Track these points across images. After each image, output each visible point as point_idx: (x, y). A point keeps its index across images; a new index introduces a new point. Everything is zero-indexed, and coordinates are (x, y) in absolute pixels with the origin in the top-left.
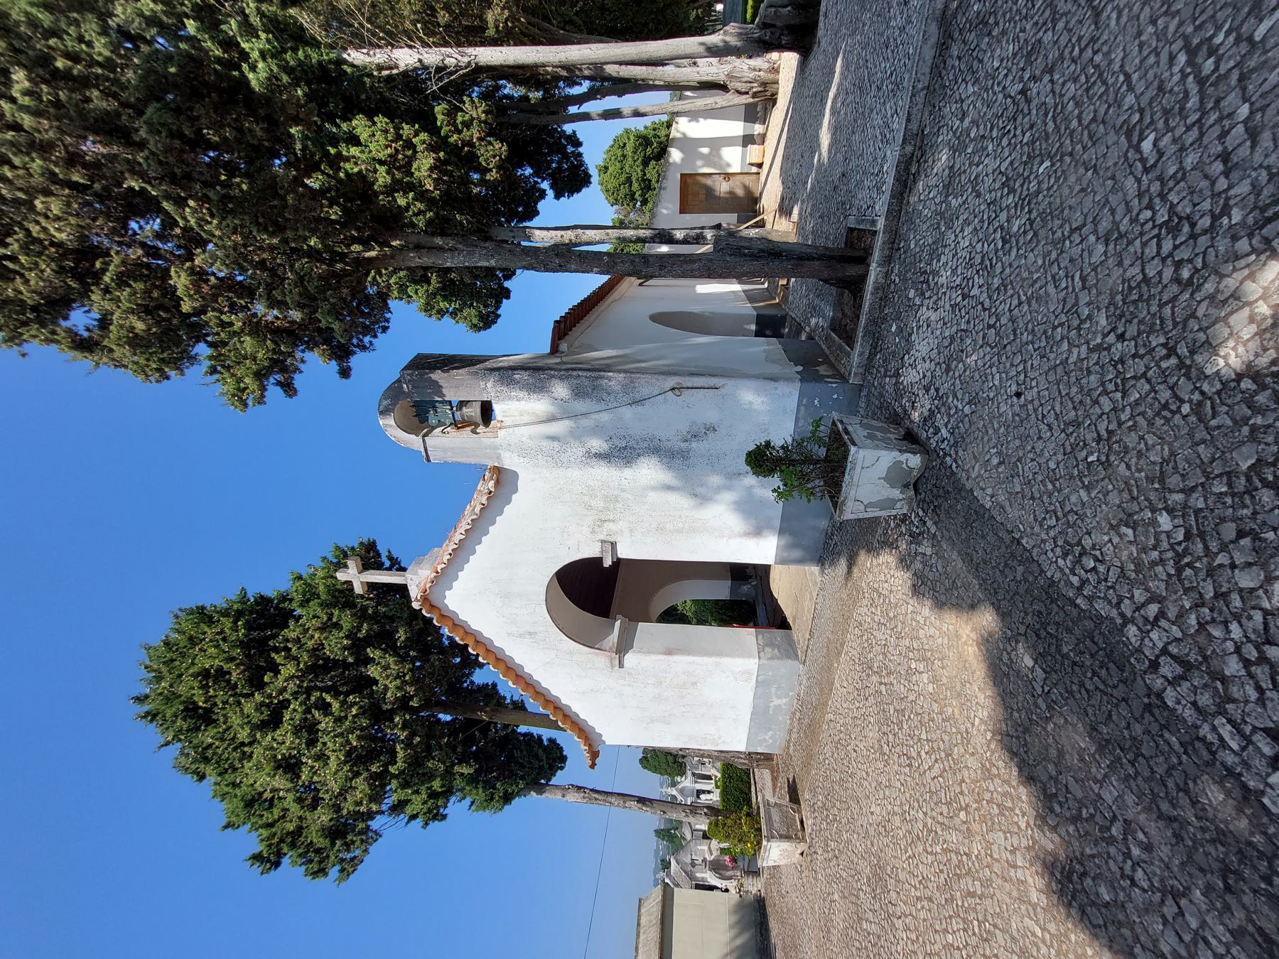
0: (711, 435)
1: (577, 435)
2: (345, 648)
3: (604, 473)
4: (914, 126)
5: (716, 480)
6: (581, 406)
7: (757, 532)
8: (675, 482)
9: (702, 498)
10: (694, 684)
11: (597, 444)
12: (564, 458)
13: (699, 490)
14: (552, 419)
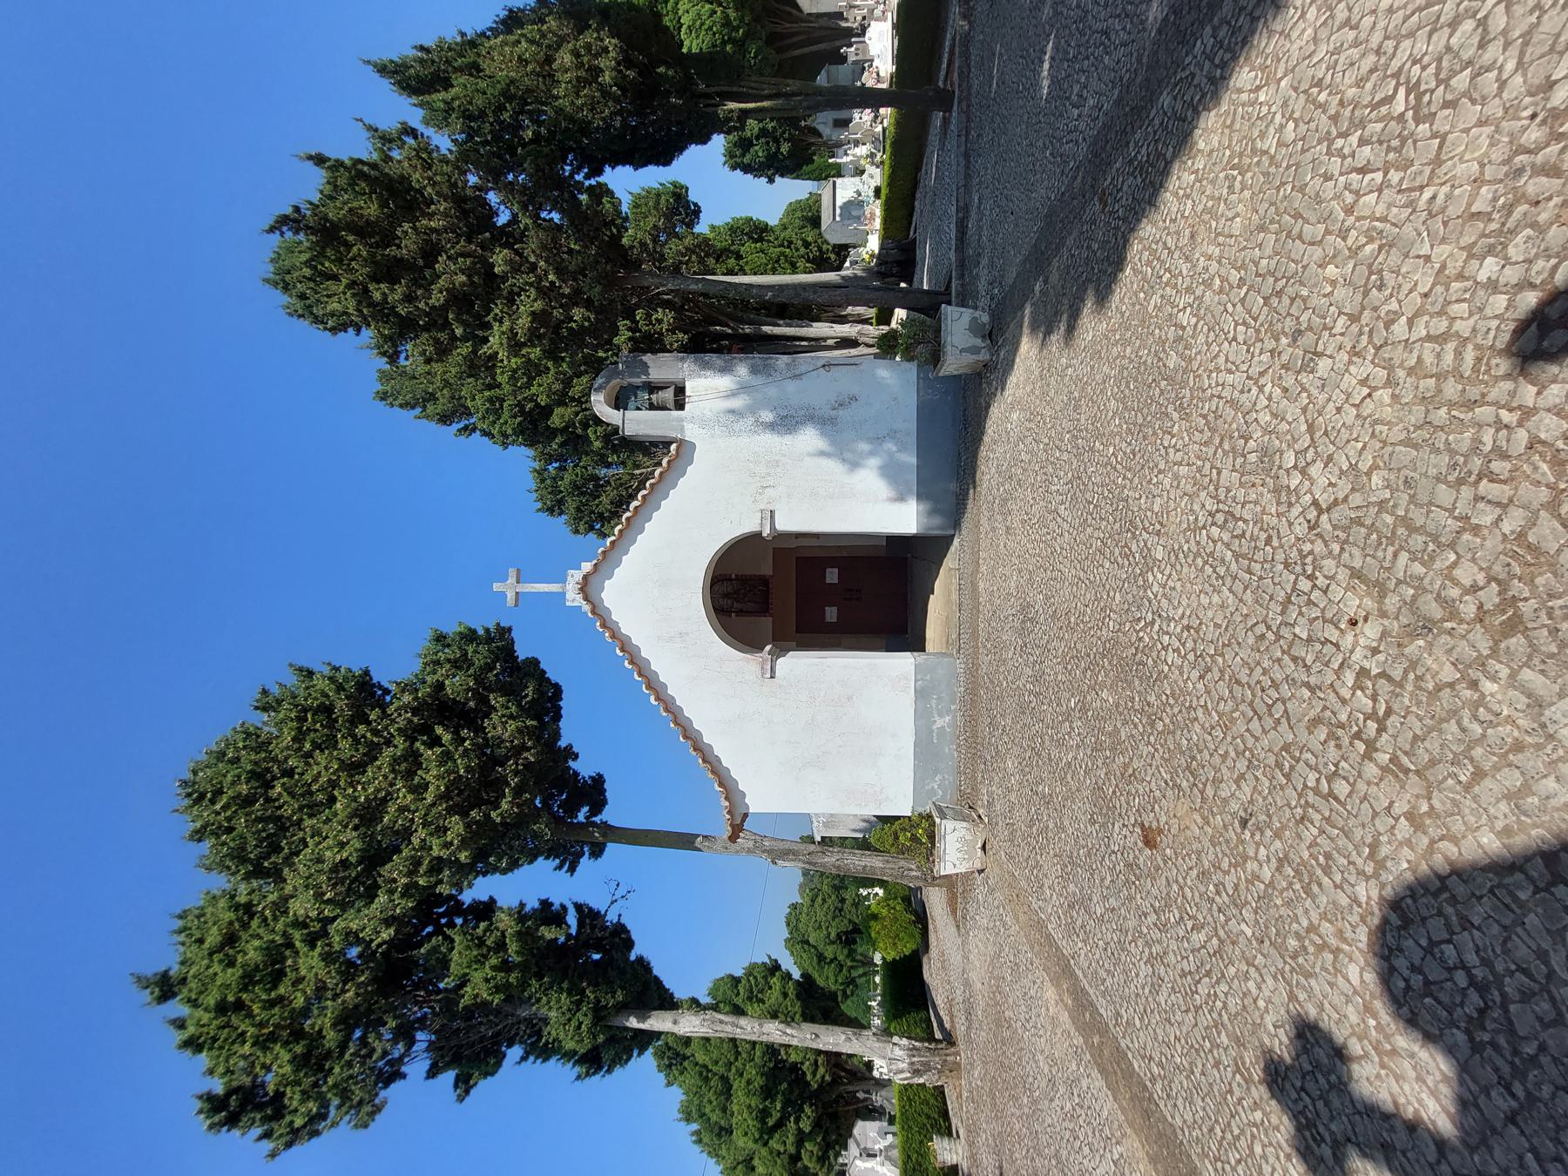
0: (854, 404)
2: (469, 689)
3: (770, 440)
4: (961, 204)
5: (864, 447)
6: (758, 380)
7: (901, 498)
9: (854, 465)
10: (850, 698)
11: (767, 416)
12: (737, 427)
13: (848, 455)
14: (733, 394)
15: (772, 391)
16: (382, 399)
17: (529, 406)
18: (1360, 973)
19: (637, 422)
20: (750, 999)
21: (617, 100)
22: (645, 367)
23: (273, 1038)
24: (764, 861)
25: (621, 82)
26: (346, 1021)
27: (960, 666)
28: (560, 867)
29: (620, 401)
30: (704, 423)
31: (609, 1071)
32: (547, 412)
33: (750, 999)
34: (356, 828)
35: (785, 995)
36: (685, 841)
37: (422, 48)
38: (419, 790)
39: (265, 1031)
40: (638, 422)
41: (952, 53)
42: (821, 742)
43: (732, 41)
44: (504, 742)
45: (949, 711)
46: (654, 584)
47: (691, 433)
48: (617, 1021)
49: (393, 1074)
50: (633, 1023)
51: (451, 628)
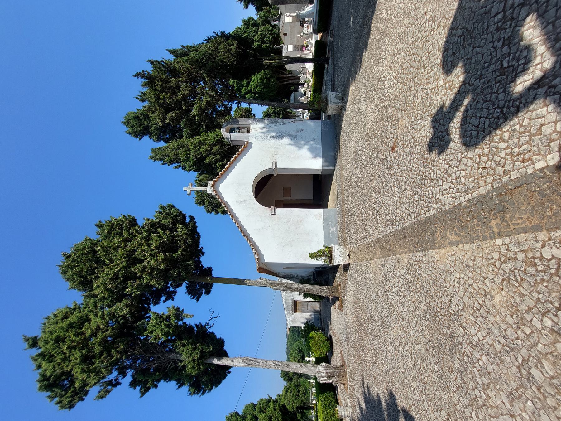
1: (268, 132)
3: (276, 142)
5: (303, 142)
6: (271, 125)
7: (315, 157)
8: (293, 143)
9: (300, 147)
10: (301, 221)
11: (273, 134)
12: (266, 138)
15: (276, 127)
16: (151, 159)
17: (198, 156)
18: (452, 145)
19: (235, 137)
20: (260, 412)
21: (235, 57)
22: (238, 121)
23: (74, 347)
24: (270, 289)
25: (237, 52)
26: (104, 342)
27: (338, 210)
28: (193, 298)
29: (231, 131)
30: (255, 137)
31: (203, 394)
32: (204, 158)
33: (260, 412)
34: (125, 258)
35: (275, 409)
36: (241, 282)
37: (183, 46)
38: (149, 245)
39: (73, 344)
40: (235, 137)
41: (329, 52)
42: (292, 237)
43: (266, 78)
44: (178, 254)
45: (335, 226)
46: (236, 186)
47: (251, 140)
48: (208, 361)
49: (115, 384)
50: (216, 361)
51: (165, 204)
